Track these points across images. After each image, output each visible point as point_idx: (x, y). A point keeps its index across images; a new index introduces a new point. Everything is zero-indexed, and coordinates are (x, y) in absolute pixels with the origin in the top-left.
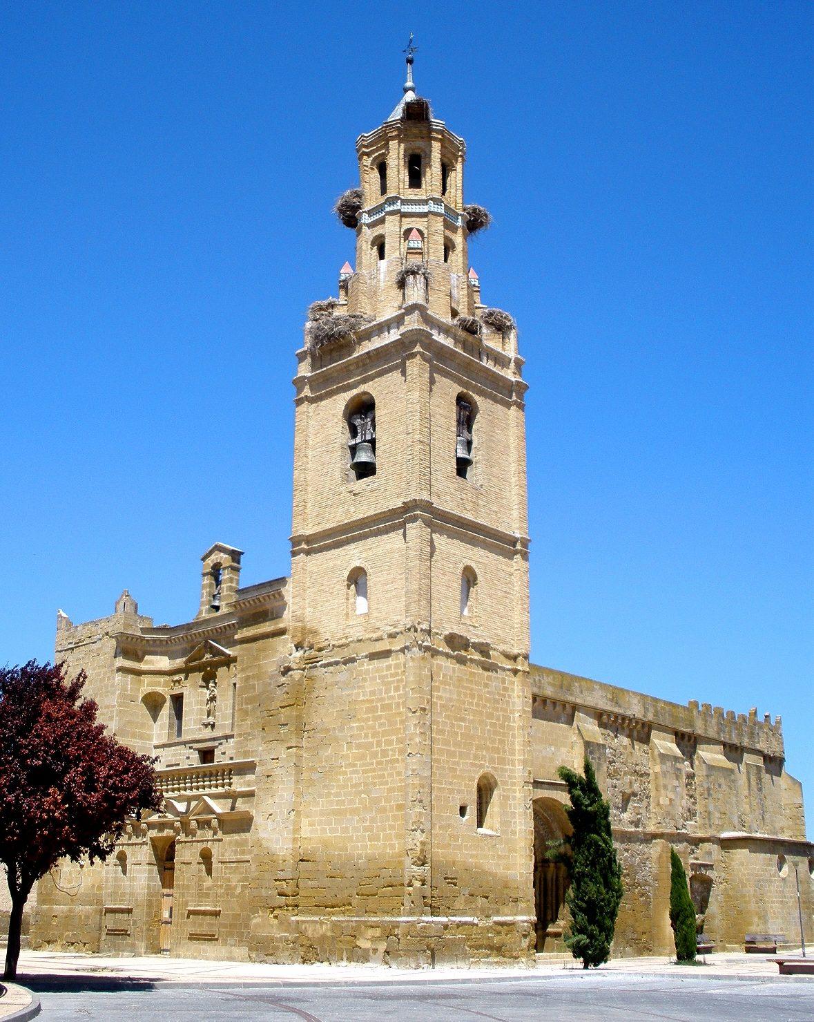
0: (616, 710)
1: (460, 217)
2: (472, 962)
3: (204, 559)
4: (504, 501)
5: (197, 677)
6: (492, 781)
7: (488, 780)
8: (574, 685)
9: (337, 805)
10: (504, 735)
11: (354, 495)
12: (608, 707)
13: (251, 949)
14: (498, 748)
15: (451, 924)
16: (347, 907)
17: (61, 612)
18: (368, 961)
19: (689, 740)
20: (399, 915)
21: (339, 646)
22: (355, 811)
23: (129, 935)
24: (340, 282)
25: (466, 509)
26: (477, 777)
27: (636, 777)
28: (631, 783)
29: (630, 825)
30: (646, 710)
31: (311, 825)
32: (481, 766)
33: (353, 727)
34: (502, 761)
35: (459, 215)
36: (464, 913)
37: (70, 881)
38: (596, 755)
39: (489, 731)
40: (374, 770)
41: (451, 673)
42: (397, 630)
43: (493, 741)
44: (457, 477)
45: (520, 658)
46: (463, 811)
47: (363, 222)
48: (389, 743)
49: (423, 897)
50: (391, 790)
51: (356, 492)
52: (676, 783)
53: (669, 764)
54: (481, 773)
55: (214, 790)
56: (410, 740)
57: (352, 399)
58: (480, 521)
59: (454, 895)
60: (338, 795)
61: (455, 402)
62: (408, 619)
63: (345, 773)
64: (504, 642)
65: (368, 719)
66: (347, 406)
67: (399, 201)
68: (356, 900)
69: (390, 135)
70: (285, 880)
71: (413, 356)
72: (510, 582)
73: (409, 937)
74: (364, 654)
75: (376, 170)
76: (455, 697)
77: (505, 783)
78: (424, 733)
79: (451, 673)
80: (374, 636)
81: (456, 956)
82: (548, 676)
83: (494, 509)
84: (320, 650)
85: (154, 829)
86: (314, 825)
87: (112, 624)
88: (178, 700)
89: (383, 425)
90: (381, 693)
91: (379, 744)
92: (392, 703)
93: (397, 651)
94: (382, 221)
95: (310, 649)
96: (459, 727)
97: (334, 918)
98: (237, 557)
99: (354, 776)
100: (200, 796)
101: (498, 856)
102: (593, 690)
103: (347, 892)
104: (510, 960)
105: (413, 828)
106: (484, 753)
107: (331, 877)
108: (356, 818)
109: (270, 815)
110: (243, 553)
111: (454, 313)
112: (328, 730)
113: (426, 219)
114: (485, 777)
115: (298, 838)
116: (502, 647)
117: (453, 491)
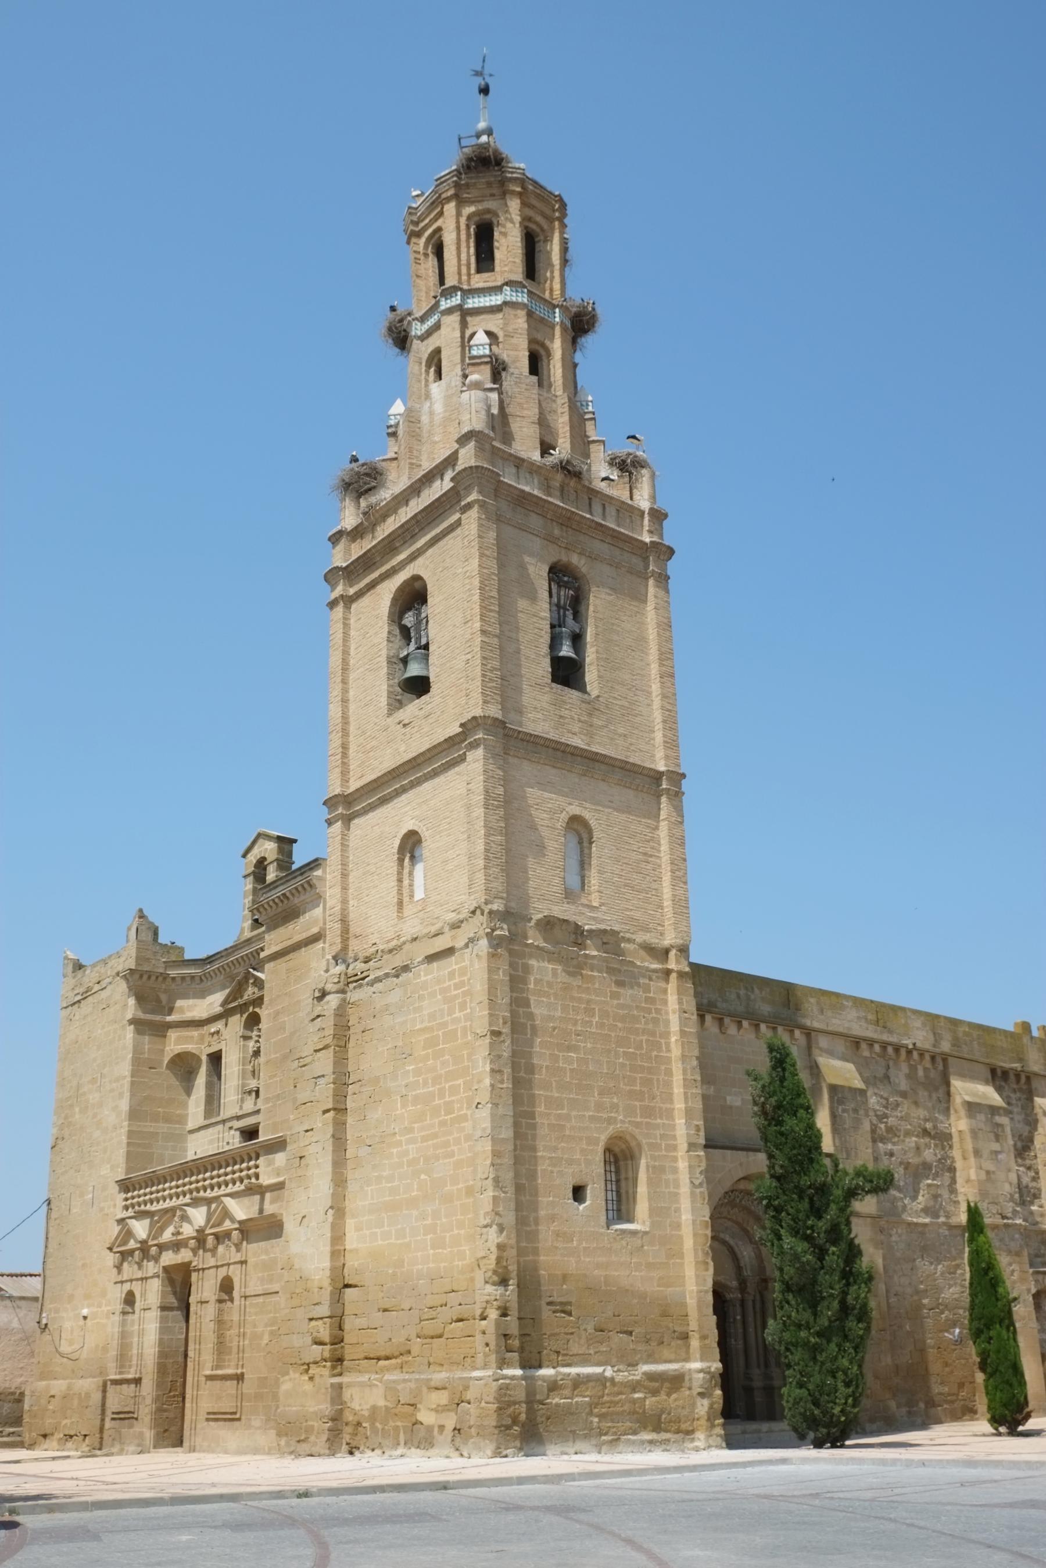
0: (885, 1037)
1: (557, 310)
3: (244, 856)
4: (638, 719)
6: (633, 1144)
11: (405, 725)
13: (279, 1435)
14: (642, 1093)
16: (405, 1358)
17: (68, 953)
18: (431, 1445)
19: (1018, 1081)
21: (390, 951)
23: (136, 1419)
24: (389, 427)
25: (569, 732)
26: (603, 1138)
27: (927, 1140)
28: (918, 1148)
29: (922, 1214)
30: (937, 1038)
31: (358, 1229)
32: (610, 1121)
33: (408, 1071)
34: (649, 1112)
36: (585, 1361)
38: (850, 1106)
39: (623, 1065)
41: (549, 977)
42: (461, 917)
45: (672, 954)
46: (578, 1193)
48: (454, 1090)
49: (505, 1335)
51: (406, 721)
52: (996, 1146)
53: (981, 1117)
54: (611, 1130)
55: (231, 1189)
57: (401, 590)
58: (595, 748)
61: (546, 575)
62: (472, 897)
64: (646, 929)
66: (394, 601)
67: (459, 293)
69: (444, 196)
70: (321, 1318)
72: (652, 839)
73: (483, 1404)
74: (420, 959)
75: (431, 256)
78: (500, 1071)
79: (549, 977)
80: (433, 929)
83: (621, 730)
84: (367, 960)
85: (167, 1250)
86: (362, 1229)
88: (216, 1059)
92: (456, 1029)
93: (461, 949)
94: (437, 326)
95: (356, 960)
98: (286, 847)
99: (411, 1146)
100: (219, 1197)
102: (843, 1007)
106: (615, 1100)
107: (385, 1310)
108: (415, 1213)
109: (304, 1217)
110: (295, 841)
111: (546, 448)
112: (377, 1080)
113: (500, 315)
114: (621, 1137)
115: (339, 1251)
116: (640, 937)
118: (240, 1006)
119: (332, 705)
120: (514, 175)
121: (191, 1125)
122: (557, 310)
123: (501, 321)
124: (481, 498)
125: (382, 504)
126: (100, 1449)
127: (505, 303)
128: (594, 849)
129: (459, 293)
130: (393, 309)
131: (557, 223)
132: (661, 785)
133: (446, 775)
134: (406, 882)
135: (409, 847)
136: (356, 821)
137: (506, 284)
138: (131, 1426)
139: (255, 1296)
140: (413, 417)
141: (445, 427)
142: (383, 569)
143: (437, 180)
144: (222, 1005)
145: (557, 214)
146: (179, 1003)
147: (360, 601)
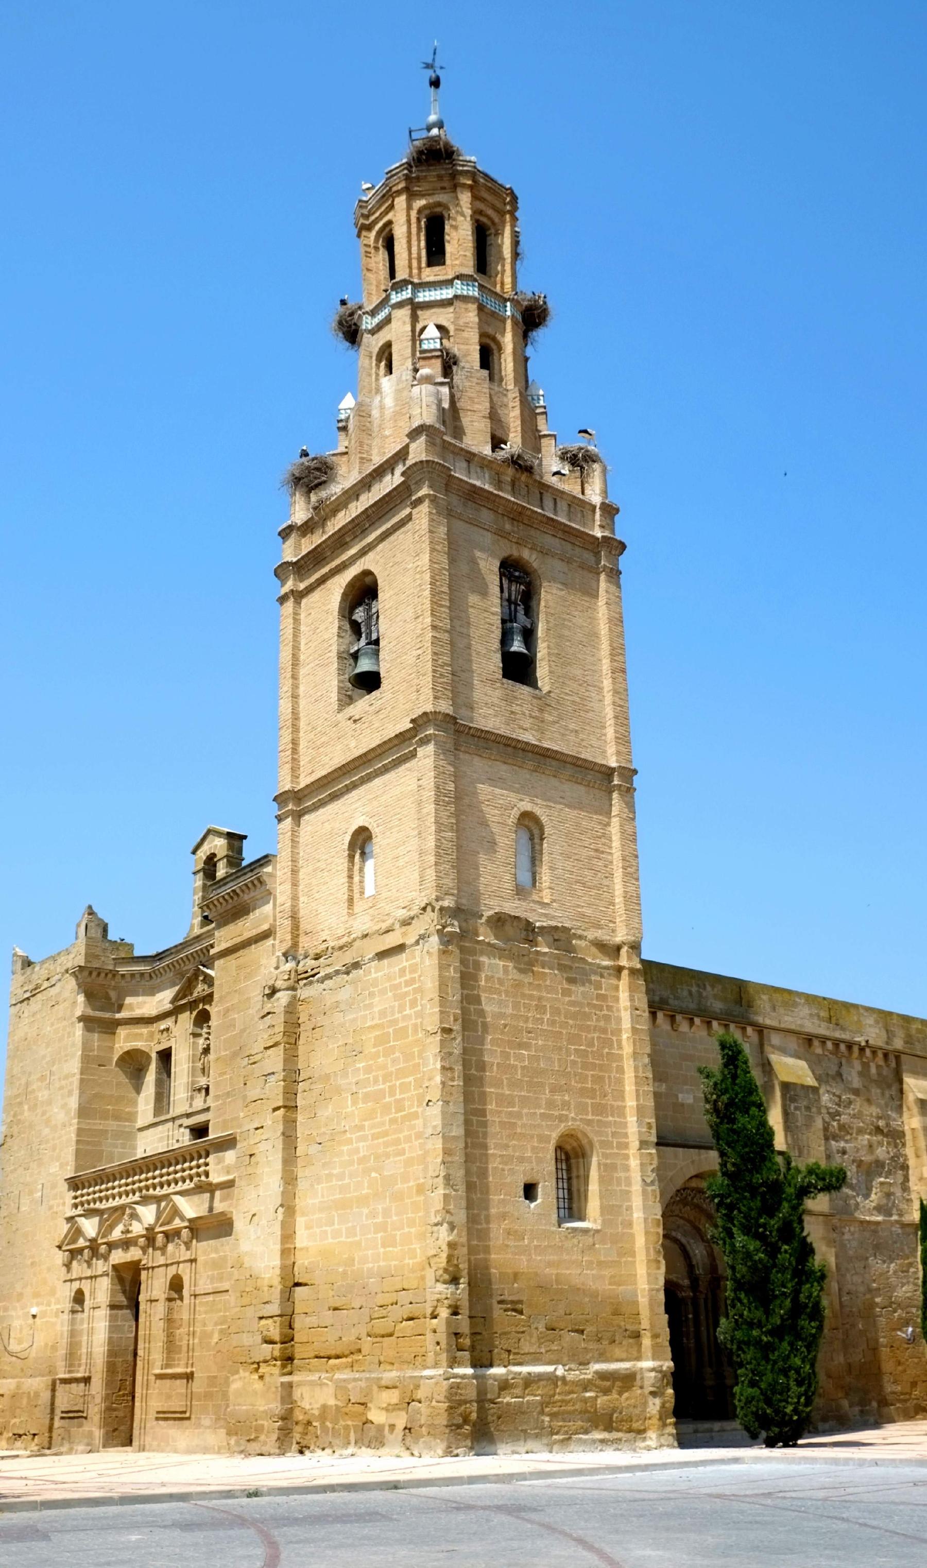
0: (838, 1034)
1: (508, 304)
2: (555, 1442)
3: (194, 852)
5: (186, 1019)
6: (585, 1142)
7: (577, 1139)
8: (760, 999)
9: (340, 1193)
10: (601, 1068)
11: (355, 721)
12: (822, 1030)
15: (513, 1379)
16: (355, 1357)
17: (17, 949)
18: (382, 1444)
20: (425, 1367)
21: (341, 948)
22: (363, 1201)
23: (86, 1418)
24: (339, 421)
26: (555, 1136)
27: (880, 1138)
28: (871, 1146)
30: (890, 1035)
32: (562, 1118)
33: (359, 1069)
34: (600, 1109)
35: (506, 300)
36: (536, 1359)
37: (20, 1342)
38: (803, 1103)
39: (574, 1063)
40: (386, 1133)
41: (501, 974)
42: (412, 913)
43: (583, 1079)
44: (505, 680)
45: (624, 950)
46: (530, 1191)
47: (364, 327)
48: (405, 1088)
49: (456, 1334)
50: (408, 1163)
51: (357, 717)
54: (562, 1128)
55: (180, 1187)
56: (430, 1079)
57: (351, 585)
58: (546, 744)
59: (518, 1329)
60: (341, 1177)
63: (350, 1141)
65: (377, 1055)
66: (345, 595)
67: (410, 287)
68: (367, 1344)
70: (271, 1317)
71: (420, 501)
73: (434, 1403)
74: (371, 956)
76: (510, 1011)
77: (606, 1144)
78: (451, 1069)
79: (501, 974)
80: (384, 926)
81: (524, 1431)
82: (713, 987)
84: (317, 957)
87: (72, 956)
89: (388, 612)
90: (393, 1014)
91: (392, 1093)
92: (407, 1027)
93: (412, 945)
94: (388, 320)
95: (306, 957)
96: (520, 1058)
97: (338, 1376)
98: (236, 843)
101: (600, 1263)
102: (795, 1005)
103: (354, 1332)
104: (628, 1435)
105: (436, 1221)
106: (566, 1098)
107: (335, 1309)
110: (245, 837)
111: (497, 442)
112: (327, 1077)
113: (451, 309)
115: (290, 1249)
116: (591, 934)
117: (496, 701)
118: (190, 1003)
119: (282, 701)
120: (465, 168)
121: (140, 1123)
122: (508, 304)
123: (452, 315)
124: (432, 492)
125: (333, 499)
126: (49, 1448)
127: (456, 297)
128: (545, 845)
129: (410, 287)
130: (343, 302)
131: (508, 216)
132: (613, 781)
133: (397, 771)
134: (356, 879)
135: (359, 843)
136: (306, 817)
137: (458, 277)
138: (80, 1426)
139: (205, 1294)
140: (363, 411)
141: (396, 421)
142: (333, 564)
143: (387, 173)
144: (172, 1002)
145: (508, 208)
146: (129, 1000)
147: (310, 596)
